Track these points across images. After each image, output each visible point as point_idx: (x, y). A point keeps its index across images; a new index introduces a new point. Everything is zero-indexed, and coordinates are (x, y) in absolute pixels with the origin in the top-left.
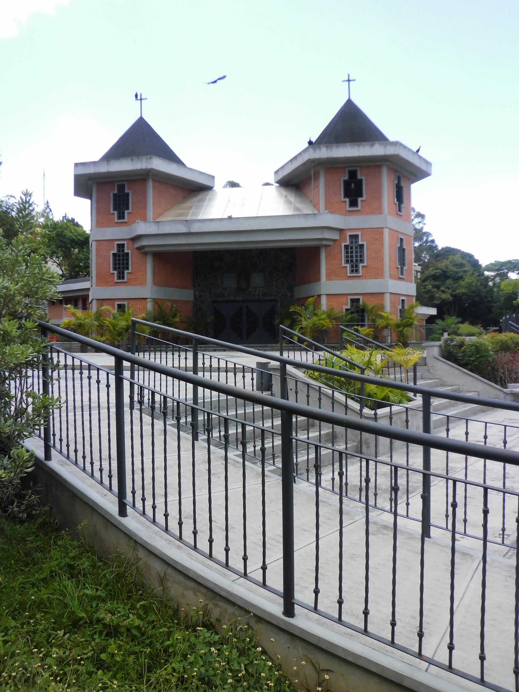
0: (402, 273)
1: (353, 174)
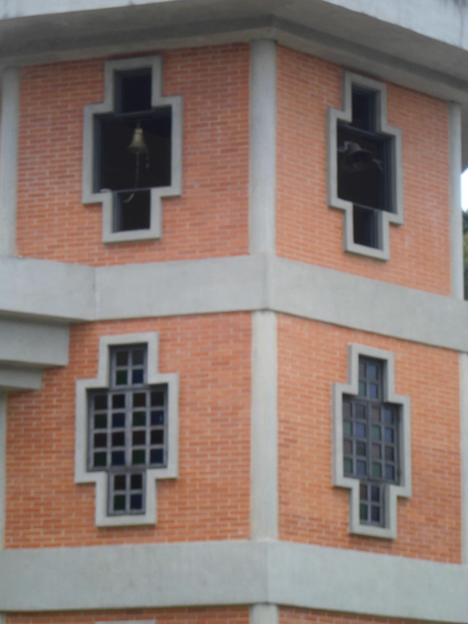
0: (374, 511)
1: (134, 88)
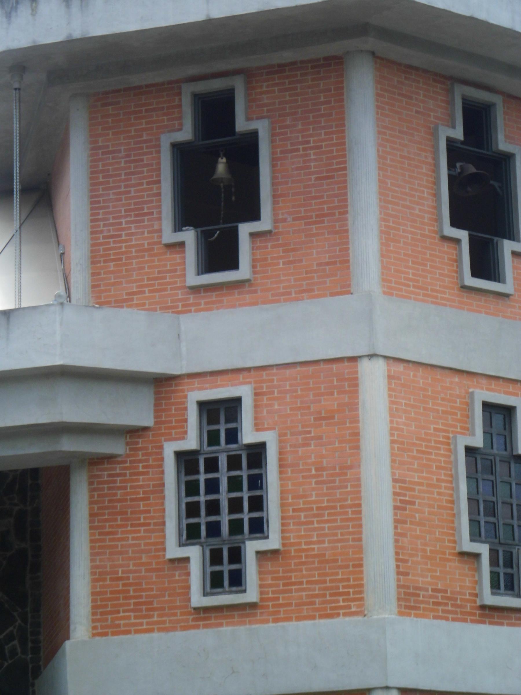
1: (215, 113)
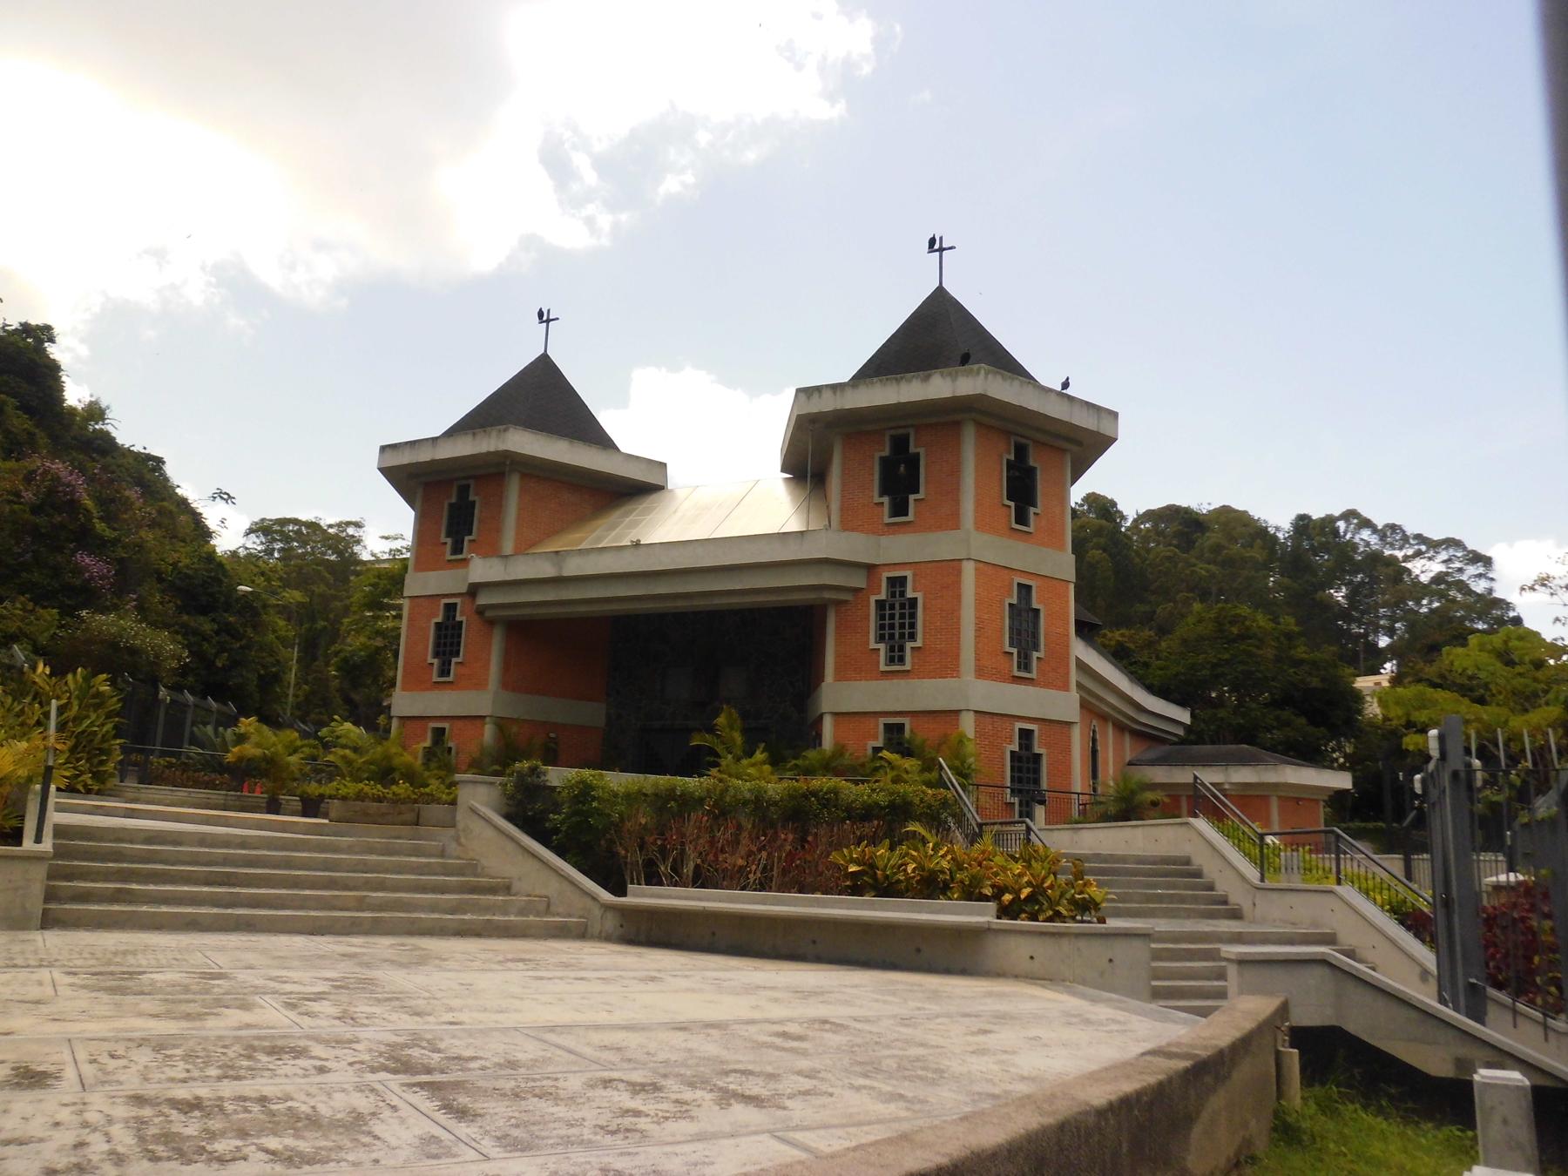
0: (1025, 664)
1: (900, 444)
